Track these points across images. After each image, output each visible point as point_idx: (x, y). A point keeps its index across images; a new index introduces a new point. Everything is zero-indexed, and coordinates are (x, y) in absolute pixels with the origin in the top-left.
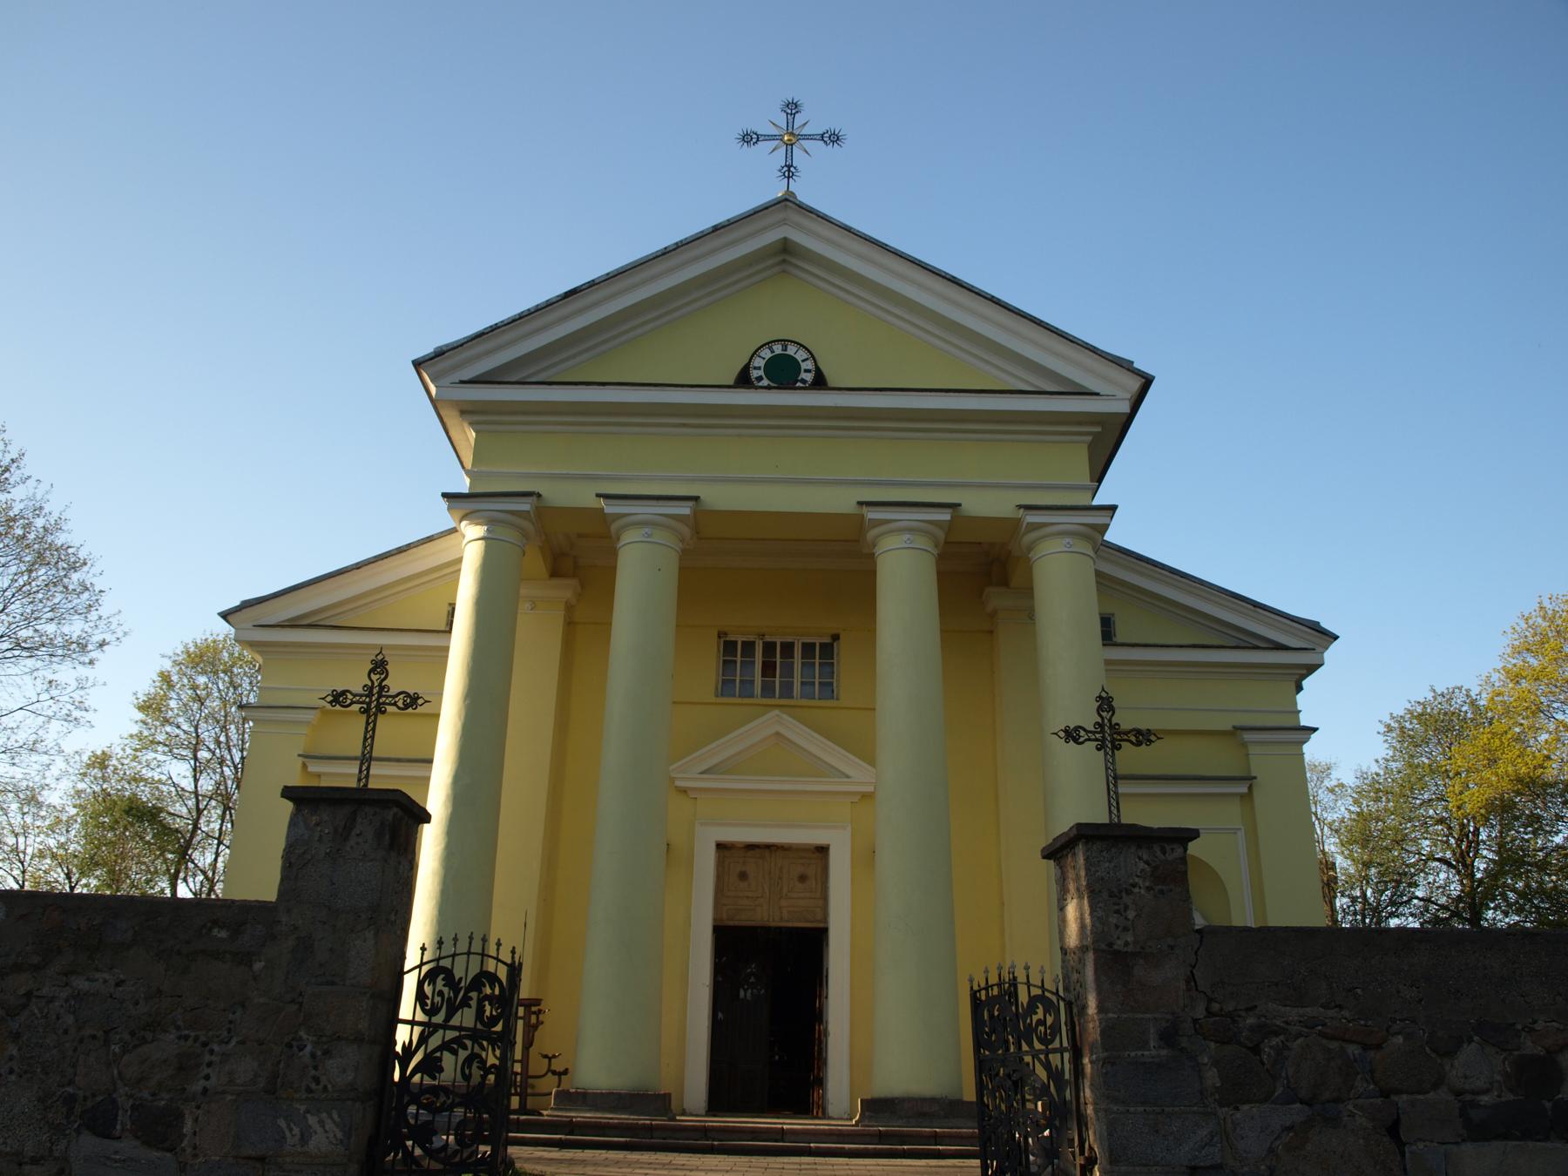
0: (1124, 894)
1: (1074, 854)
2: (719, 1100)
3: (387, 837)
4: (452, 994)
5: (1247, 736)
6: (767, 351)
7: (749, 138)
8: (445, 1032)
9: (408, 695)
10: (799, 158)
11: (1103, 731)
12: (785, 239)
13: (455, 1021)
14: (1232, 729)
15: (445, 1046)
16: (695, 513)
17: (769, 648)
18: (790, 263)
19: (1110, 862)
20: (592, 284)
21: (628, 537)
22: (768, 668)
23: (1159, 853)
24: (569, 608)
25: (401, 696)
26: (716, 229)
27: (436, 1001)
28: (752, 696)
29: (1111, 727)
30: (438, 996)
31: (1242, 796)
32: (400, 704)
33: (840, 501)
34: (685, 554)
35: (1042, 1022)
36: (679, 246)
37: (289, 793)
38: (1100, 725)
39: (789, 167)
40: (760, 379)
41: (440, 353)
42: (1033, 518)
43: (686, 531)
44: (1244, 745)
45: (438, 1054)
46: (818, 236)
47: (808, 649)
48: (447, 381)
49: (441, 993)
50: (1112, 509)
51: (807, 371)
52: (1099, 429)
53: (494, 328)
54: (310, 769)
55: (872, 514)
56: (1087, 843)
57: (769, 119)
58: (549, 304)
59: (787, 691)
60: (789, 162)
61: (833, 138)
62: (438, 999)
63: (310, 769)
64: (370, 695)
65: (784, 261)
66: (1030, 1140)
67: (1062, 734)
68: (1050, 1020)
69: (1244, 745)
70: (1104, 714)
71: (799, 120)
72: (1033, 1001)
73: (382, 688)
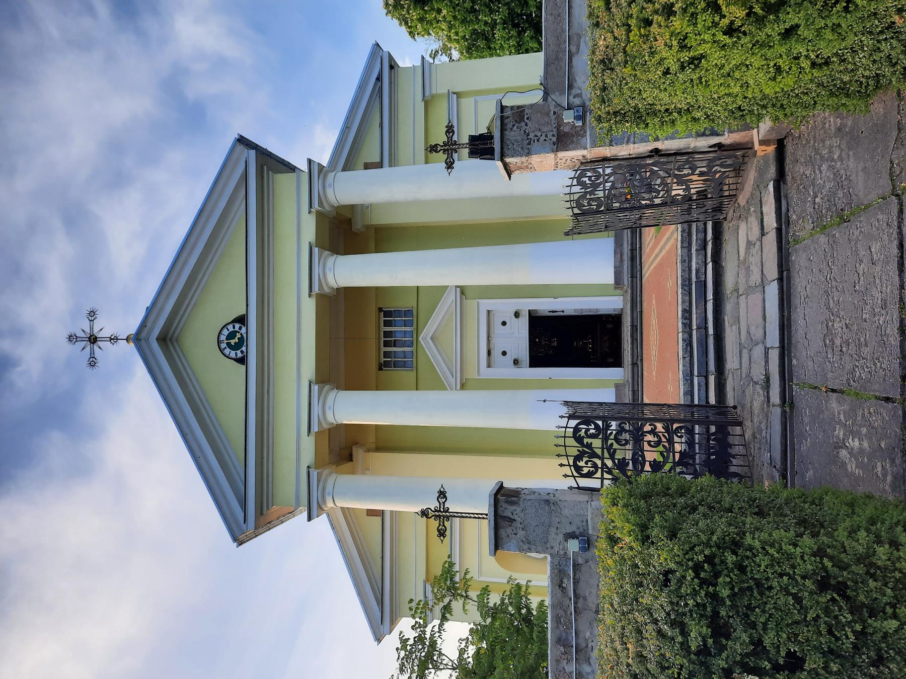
0: (529, 137)
1: (510, 163)
3: (513, 499)
4: (586, 455)
5: (427, 94)
6: (225, 351)
9: (439, 496)
10: (106, 333)
11: (447, 150)
12: (157, 339)
13: (599, 452)
14: (423, 102)
15: (612, 457)
16: (317, 383)
18: (172, 336)
19: (514, 144)
23: (509, 120)
25: (440, 500)
26: (333, 528)
27: (590, 465)
29: (445, 145)
30: (587, 464)
32: (444, 500)
33: (309, 307)
34: (339, 388)
35: (590, 177)
38: (444, 151)
39: (111, 339)
40: (242, 352)
43: (327, 387)
45: (616, 461)
49: (586, 463)
50: (310, 161)
51: (234, 327)
52: (270, 172)
55: (316, 289)
56: (504, 156)
60: (108, 339)
62: (590, 464)
64: (439, 516)
65: (171, 340)
67: (450, 170)
68: (589, 174)
69: (433, 97)
70: (439, 149)
72: (580, 183)
73: (436, 511)
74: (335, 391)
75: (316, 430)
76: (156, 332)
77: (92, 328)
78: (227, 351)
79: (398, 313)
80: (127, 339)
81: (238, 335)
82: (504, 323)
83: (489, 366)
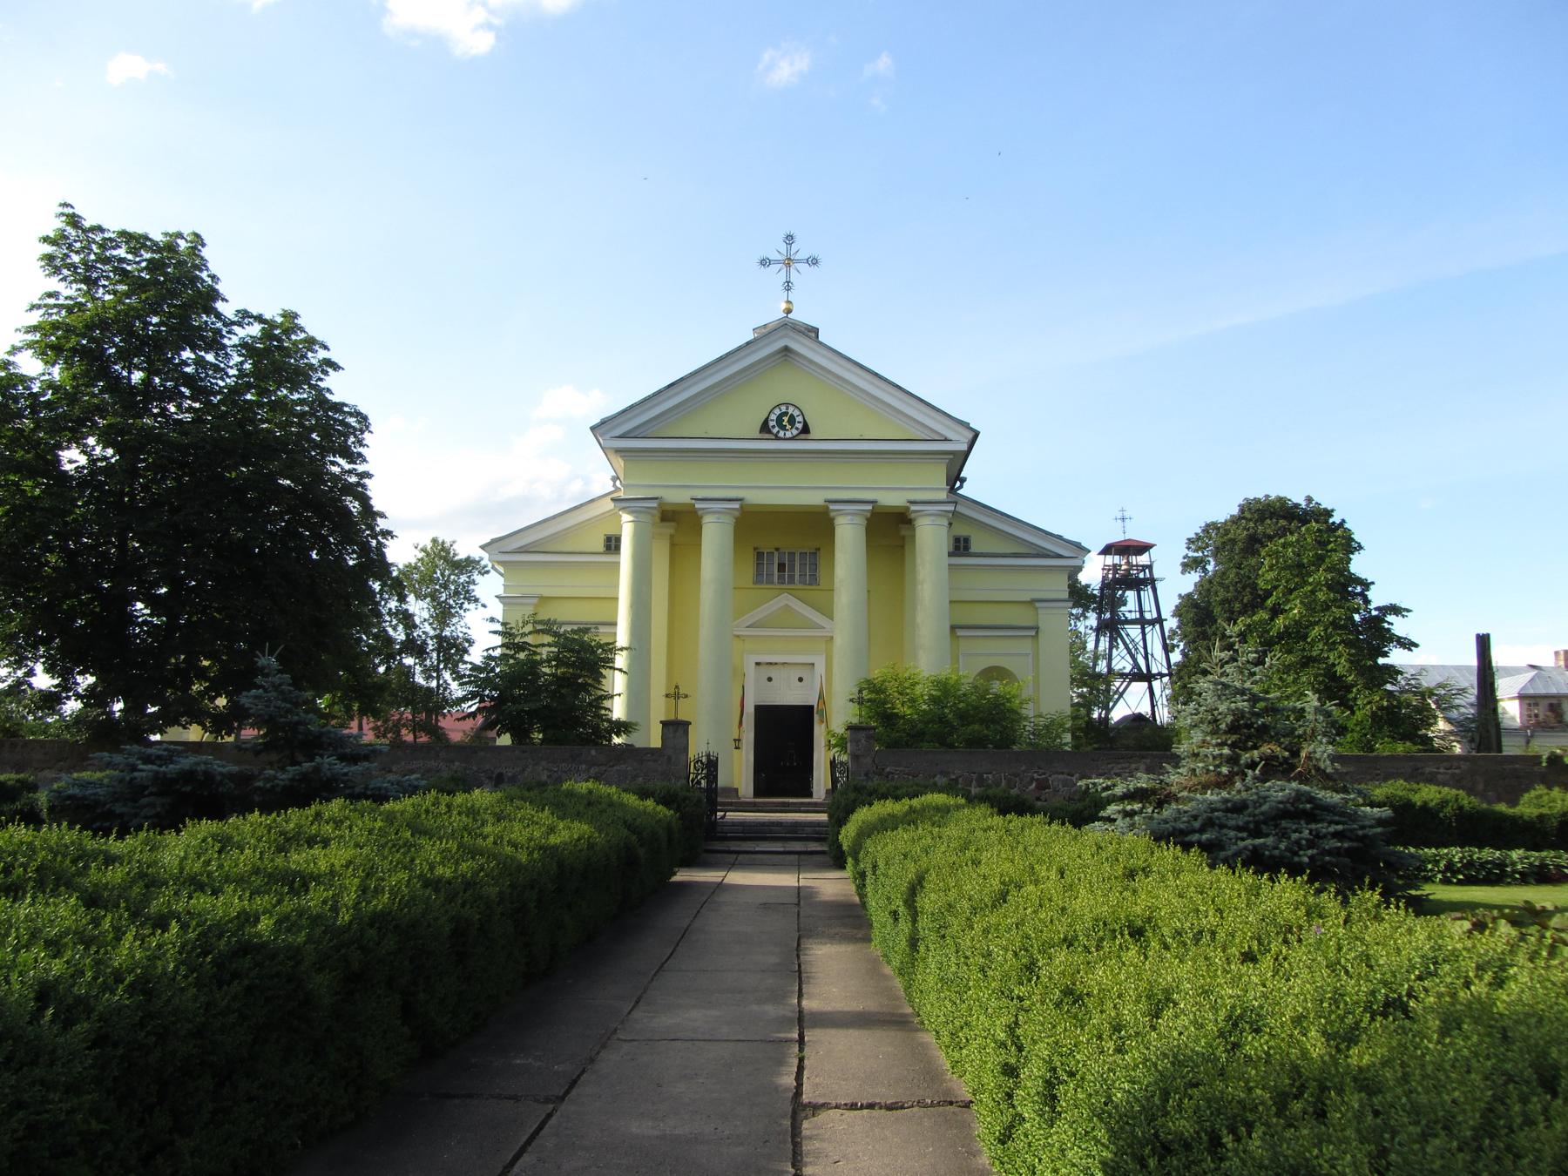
2: (757, 793)
5: (1037, 605)
7: (764, 262)
16: (741, 506)
17: (782, 554)
20: (682, 379)
21: (707, 519)
22: (781, 567)
24: (672, 537)
28: (772, 583)
33: (814, 499)
36: (728, 355)
37: (661, 722)
39: (788, 282)
41: (603, 422)
44: (1037, 609)
47: (803, 555)
48: (608, 436)
52: (951, 457)
53: (632, 407)
57: (776, 249)
58: (660, 392)
59: (792, 580)
61: (813, 262)
69: (1037, 609)
71: (794, 248)
75: (697, 506)
77: (799, 261)
78: (777, 412)
80: (789, 302)
82: (801, 680)
83: (758, 664)
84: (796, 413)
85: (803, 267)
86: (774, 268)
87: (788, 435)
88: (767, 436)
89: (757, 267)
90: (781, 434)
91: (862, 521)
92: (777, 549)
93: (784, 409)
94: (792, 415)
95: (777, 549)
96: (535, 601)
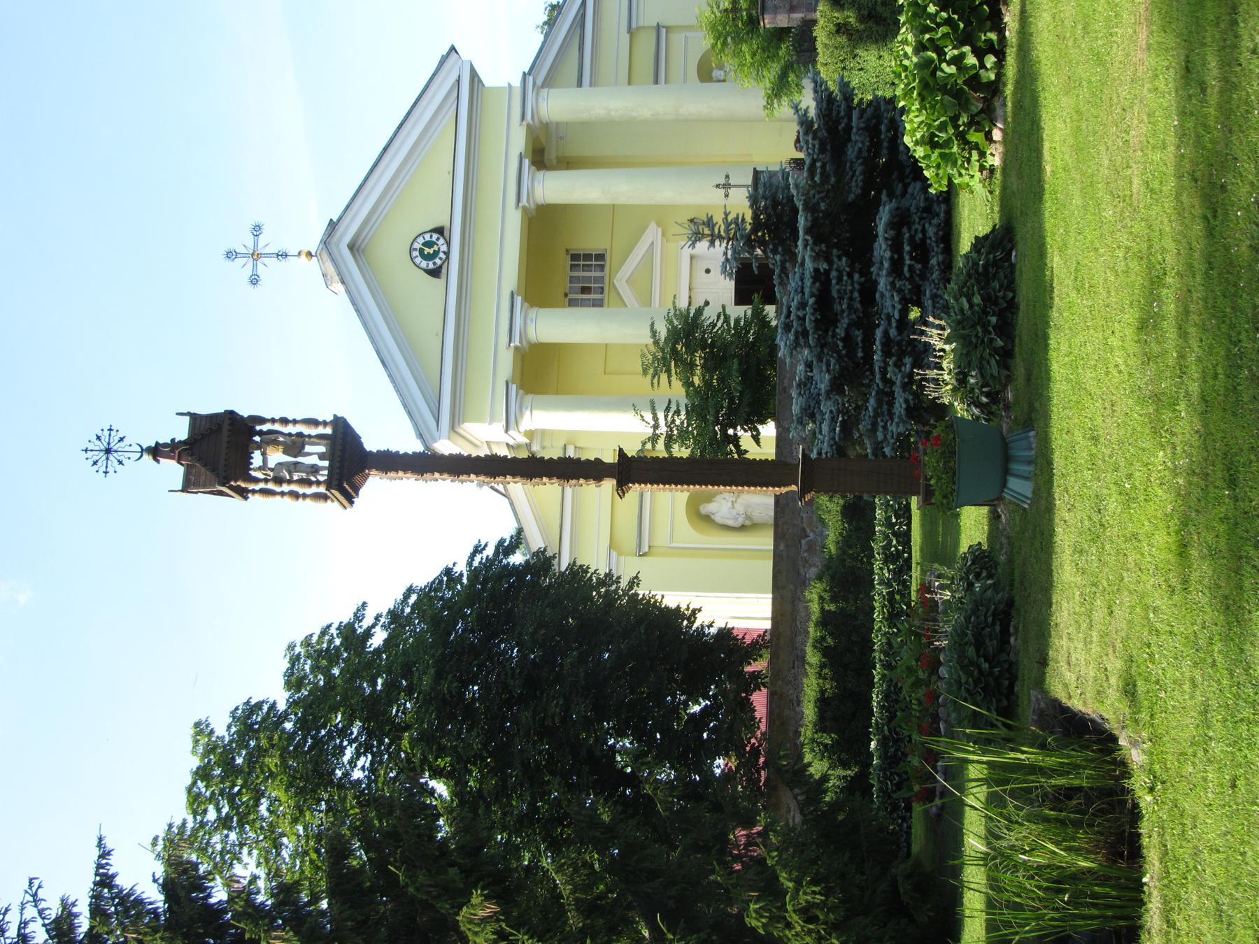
5: (634, 25)
7: (254, 280)
8: (766, 619)
17: (571, 290)
28: (602, 300)
31: (667, 32)
36: (354, 303)
39: (278, 255)
42: (529, 116)
46: (347, 228)
51: (431, 237)
54: (646, 550)
57: (242, 269)
58: (390, 376)
63: (646, 550)
66: (646, 933)
69: (638, 28)
71: (241, 250)
74: (535, 310)
75: (517, 343)
76: (347, 239)
77: (256, 244)
78: (418, 260)
79: (588, 257)
81: (436, 248)
84: (421, 240)
85: (262, 240)
86: (261, 270)
87: (444, 248)
88: (444, 271)
89: (258, 288)
90: (442, 255)
91: (533, 312)
92: (566, 295)
93: (416, 253)
94: (423, 244)
95: (566, 295)
96: (614, 554)
